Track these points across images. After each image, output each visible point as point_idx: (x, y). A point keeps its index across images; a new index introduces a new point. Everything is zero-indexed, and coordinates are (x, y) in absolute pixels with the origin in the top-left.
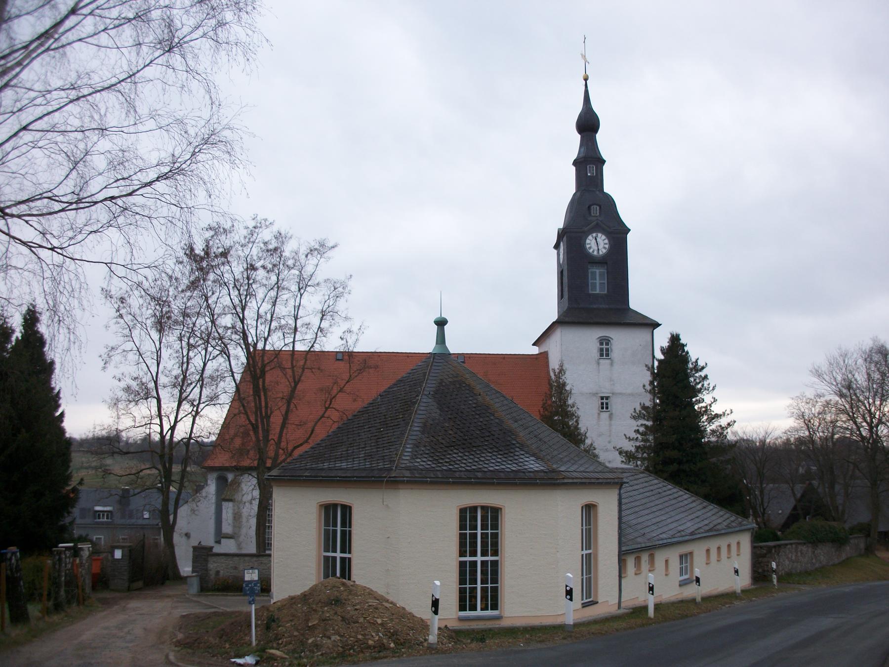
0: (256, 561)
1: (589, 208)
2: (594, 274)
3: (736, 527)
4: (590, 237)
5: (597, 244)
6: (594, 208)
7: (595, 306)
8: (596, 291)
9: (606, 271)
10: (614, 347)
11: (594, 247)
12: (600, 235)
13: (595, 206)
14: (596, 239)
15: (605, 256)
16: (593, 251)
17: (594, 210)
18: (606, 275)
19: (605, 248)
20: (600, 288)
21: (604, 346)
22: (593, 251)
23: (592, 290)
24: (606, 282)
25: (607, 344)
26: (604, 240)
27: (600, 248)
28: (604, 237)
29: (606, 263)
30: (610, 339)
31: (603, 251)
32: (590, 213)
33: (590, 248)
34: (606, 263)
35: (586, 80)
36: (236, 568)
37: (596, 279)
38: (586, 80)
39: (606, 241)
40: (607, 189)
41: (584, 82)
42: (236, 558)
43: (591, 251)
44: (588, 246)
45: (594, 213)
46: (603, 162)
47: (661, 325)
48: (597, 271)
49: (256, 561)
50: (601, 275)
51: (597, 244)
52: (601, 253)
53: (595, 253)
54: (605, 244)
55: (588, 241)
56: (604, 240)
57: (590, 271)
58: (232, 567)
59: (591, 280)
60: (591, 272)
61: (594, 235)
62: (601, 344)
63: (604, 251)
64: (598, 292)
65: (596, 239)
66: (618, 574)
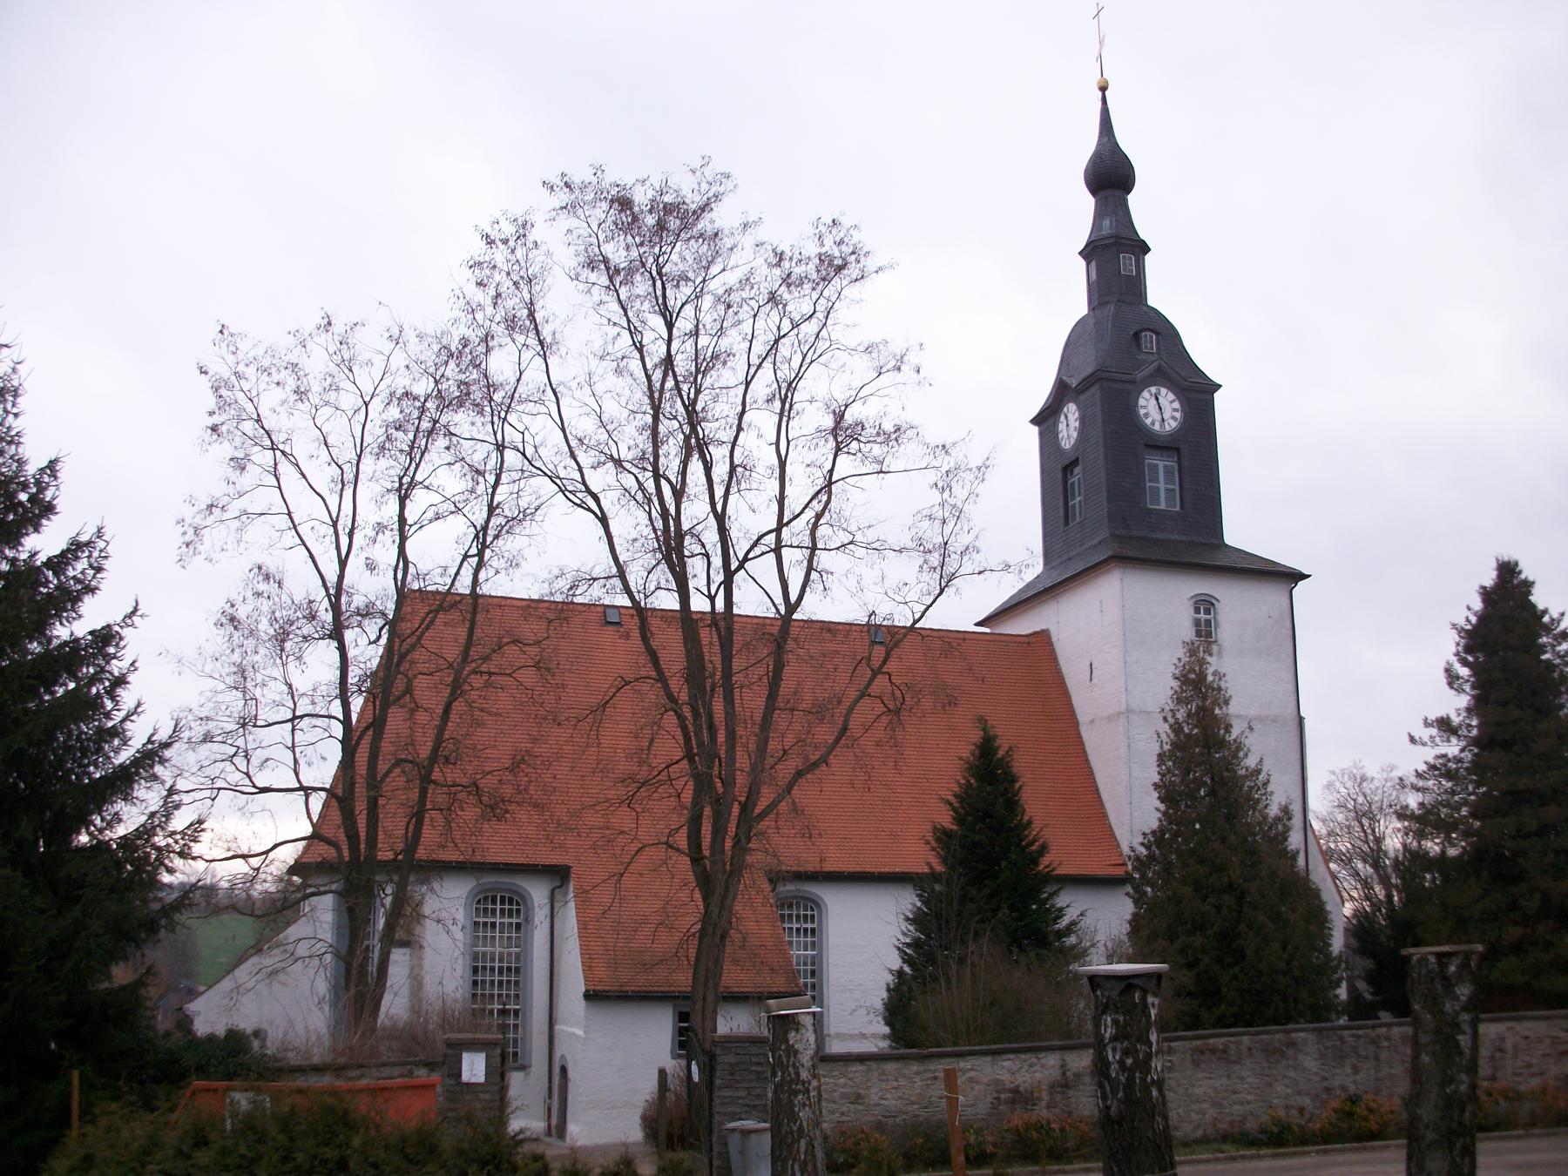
0: (917, 1073)
1: (1136, 336)
2: (1154, 468)
3: (952, 995)
4: (1145, 394)
5: (1160, 408)
6: (1146, 336)
7: (1160, 536)
8: (1159, 505)
9: (1176, 465)
10: (1221, 618)
11: (1155, 414)
12: (1163, 391)
13: (1148, 333)
14: (1157, 399)
15: (1175, 435)
16: (1153, 424)
17: (1146, 342)
18: (1177, 474)
19: (1173, 418)
20: (1167, 499)
21: (1202, 616)
22: (1153, 424)
23: (1152, 504)
24: (1177, 487)
25: (1207, 612)
26: (1172, 402)
27: (1166, 417)
28: (1171, 396)
29: (1178, 450)
30: (1214, 601)
31: (1171, 425)
32: (1139, 346)
33: (1147, 415)
34: (1178, 450)
35: (1103, 89)
36: (857, 1099)
37: (1158, 481)
38: (1103, 89)
39: (1176, 405)
40: (1152, 301)
41: (1100, 94)
42: (857, 1067)
43: (1148, 422)
44: (1142, 412)
45: (1146, 347)
46: (1144, 248)
47: (1507, 570)
48: (1161, 464)
49: (917, 1073)
50: (1168, 471)
51: (1160, 408)
52: (1168, 428)
53: (1157, 427)
54: (1174, 410)
55: (1142, 402)
56: (1172, 402)
57: (1147, 461)
58: (845, 1096)
59: (1150, 481)
60: (1149, 465)
61: (1153, 389)
62: (1197, 611)
63: (1174, 424)
64: (1163, 506)
65: (1157, 399)
66: (570, 1085)
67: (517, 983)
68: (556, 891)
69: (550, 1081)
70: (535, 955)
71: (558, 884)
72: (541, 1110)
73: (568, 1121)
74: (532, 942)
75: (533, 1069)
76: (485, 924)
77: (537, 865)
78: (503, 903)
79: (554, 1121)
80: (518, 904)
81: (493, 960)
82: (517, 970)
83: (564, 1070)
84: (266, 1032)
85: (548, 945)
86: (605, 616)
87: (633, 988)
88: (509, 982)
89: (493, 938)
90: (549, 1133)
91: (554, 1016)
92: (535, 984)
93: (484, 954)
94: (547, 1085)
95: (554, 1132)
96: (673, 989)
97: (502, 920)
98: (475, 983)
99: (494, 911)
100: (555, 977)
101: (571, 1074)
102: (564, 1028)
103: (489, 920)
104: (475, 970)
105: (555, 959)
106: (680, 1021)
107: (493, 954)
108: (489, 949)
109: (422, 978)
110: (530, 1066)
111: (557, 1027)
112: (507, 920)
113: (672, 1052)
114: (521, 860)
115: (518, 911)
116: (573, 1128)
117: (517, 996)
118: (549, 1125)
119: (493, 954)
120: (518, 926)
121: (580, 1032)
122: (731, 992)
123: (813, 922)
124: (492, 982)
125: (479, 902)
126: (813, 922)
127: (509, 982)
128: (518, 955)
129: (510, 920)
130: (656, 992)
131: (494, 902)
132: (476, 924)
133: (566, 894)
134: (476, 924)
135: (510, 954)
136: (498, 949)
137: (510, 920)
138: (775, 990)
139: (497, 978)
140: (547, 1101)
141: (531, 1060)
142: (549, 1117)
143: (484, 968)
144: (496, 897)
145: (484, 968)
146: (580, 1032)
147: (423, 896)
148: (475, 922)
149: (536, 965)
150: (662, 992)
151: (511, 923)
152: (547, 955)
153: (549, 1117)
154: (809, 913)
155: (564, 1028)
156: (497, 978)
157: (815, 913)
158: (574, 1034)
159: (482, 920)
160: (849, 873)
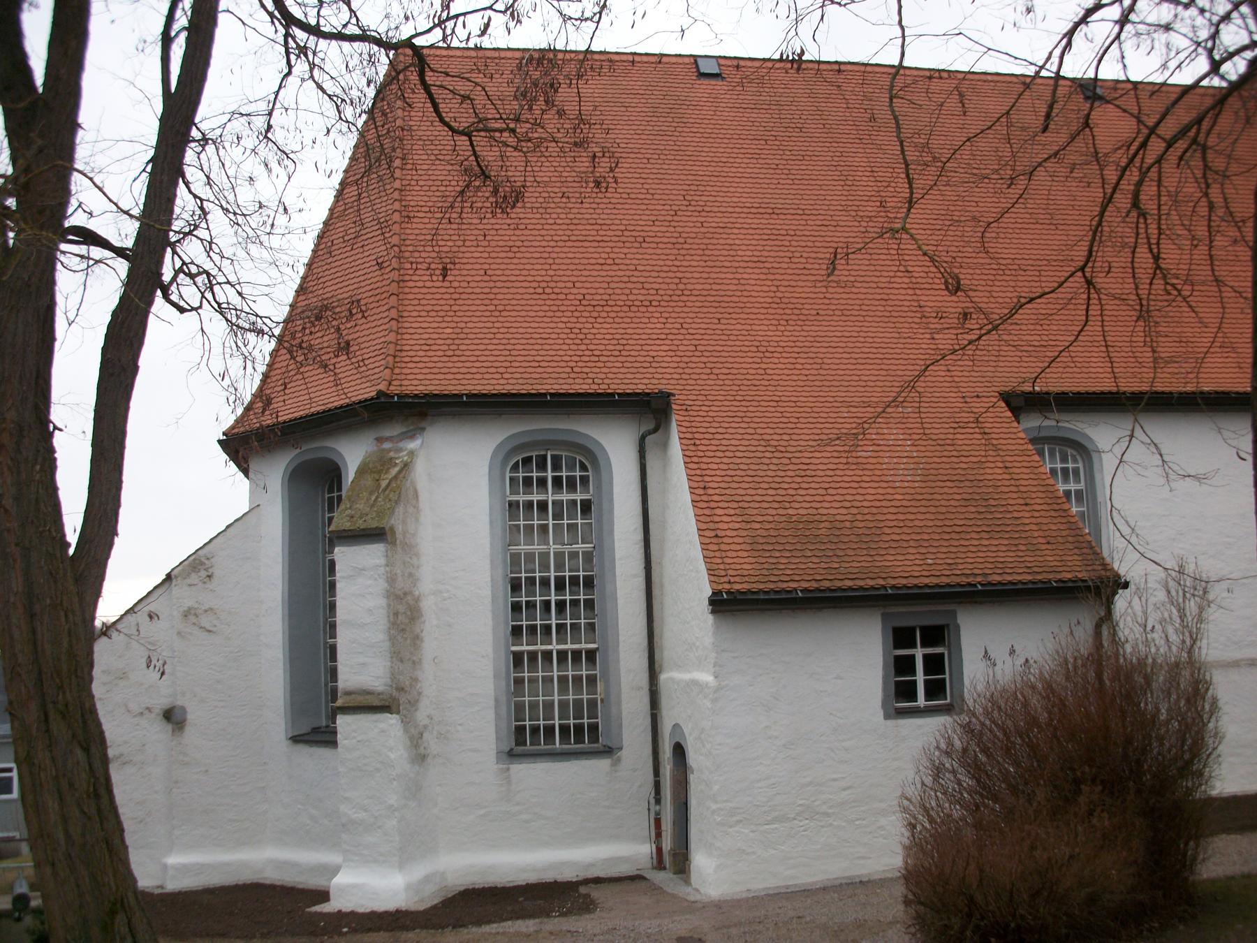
66: (692, 778)
67: (590, 604)
68: (649, 439)
69: (657, 772)
70: (618, 555)
71: (651, 426)
72: (643, 824)
73: (693, 845)
74: (611, 532)
75: (624, 753)
76: (529, 505)
77: (612, 395)
78: (556, 467)
79: (667, 844)
80: (583, 467)
81: (545, 566)
82: (589, 583)
83: (679, 751)
84: (183, 709)
85: (640, 536)
86: (697, 67)
87: (805, 585)
88: (575, 603)
89: (544, 529)
90: (660, 865)
91: (657, 657)
92: (621, 602)
93: (530, 557)
94: (651, 778)
95: (667, 859)
96: (882, 582)
97: (558, 497)
98: (516, 607)
99: (542, 482)
100: (656, 592)
101: (693, 758)
102: (676, 675)
103: (535, 498)
104: (515, 586)
105: (653, 558)
106: (897, 645)
107: (544, 556)
108: (537, 548)
109: (417, 600)
110: (621, 749)
111: (663, 677)
112: (565, 497)
113: (885, 705)
114: (583, 387)
115: (585, 480)
116: (702, 861)
117: (591, 627)
118: (659, 850)
119: (544, 556)
120: (586, 507)
121: (706, 677)
122: (990, 584)
123: (1077, 481)
124: (547, 604)
125: (515, 467)
126: (1077, 481)
127: (575, 603)
128: (588, 556)
129: (572, 497)
130: (851, 589)
131: (542, 465)
132: (513, 506)
133: (665, 445)
134: (513, 506)
135: (573, 555)
136: (553, 548)
137: (572, 497)
138: (1069, 576)
139: (553, 598)
140: (654, 808)
141: (620, 735)
142: (659, 835)
143: (531, 581)
144: (545, 457)
145: (531, 581)
146: (706, 677)
147: (412, 453)
148: (511, 504)
149: (619, 570)
150: (861, 588)
151: (574, 502)
152: (640, 581)
153: (659, 835)
154: (1070, 465)
155: (676, 675)
156: (553, 598)
157: (1080, 465)
158: (695, 682)
159: (522, 498)
160: (1133, 393)
